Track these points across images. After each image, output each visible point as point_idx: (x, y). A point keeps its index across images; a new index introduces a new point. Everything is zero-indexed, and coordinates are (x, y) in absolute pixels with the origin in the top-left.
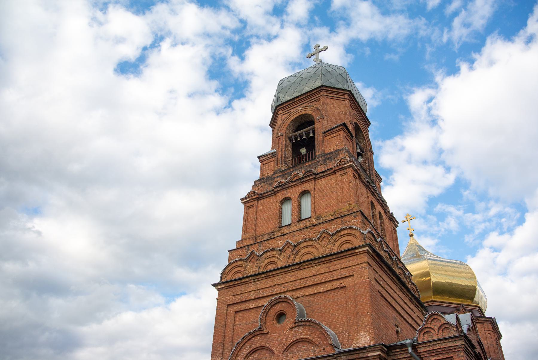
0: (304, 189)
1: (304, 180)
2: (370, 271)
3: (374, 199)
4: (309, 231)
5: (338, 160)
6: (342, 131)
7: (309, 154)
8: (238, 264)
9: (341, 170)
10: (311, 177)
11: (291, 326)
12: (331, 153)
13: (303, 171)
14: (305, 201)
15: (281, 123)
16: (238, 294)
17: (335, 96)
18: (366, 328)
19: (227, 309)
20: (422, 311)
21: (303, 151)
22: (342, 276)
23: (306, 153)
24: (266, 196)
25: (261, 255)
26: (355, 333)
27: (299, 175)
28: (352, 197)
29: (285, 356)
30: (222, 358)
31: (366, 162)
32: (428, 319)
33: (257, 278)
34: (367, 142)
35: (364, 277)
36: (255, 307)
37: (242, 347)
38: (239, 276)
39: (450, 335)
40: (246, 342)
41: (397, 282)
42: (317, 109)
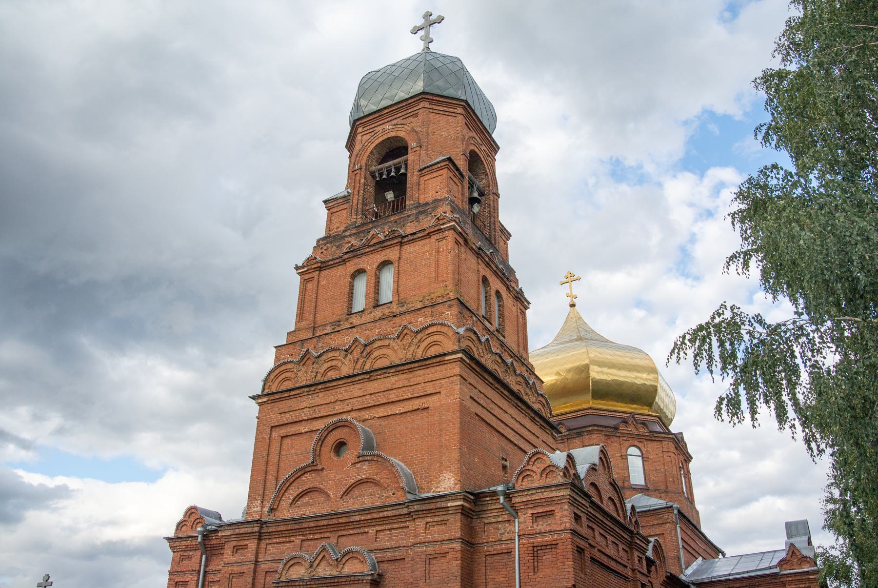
0: (383, 259)
1: (386, 244)
2: (464, 387)
3: (489, 271)
5: (436, 216)
6: (446, 170)
7: (398, 201)
10: (396, 241)
11: (353, 461)
12: (427, 204)
13: (386, 229)
15: (360, 148)
17: (442, 109)
18: (450, 467)
19: (271, 433)
20: (552, 434)
21: (390, 196)
22: (426, 393)
23: (393, 199)
24: (332, 265)
25: (319, 357)
26: (437, 473)
27: (379, 235)
28: (450, 276)
30: (262, 502)
31: (487, 210)
32: (531, 458)
33: (312, 389)
34: (490, 179)
35: (454, 395)
37: (288, 487)
38: (288, 385)
39: (555, 482)
40: (293, 481)
41: (510, 397)
42: (413, 130)
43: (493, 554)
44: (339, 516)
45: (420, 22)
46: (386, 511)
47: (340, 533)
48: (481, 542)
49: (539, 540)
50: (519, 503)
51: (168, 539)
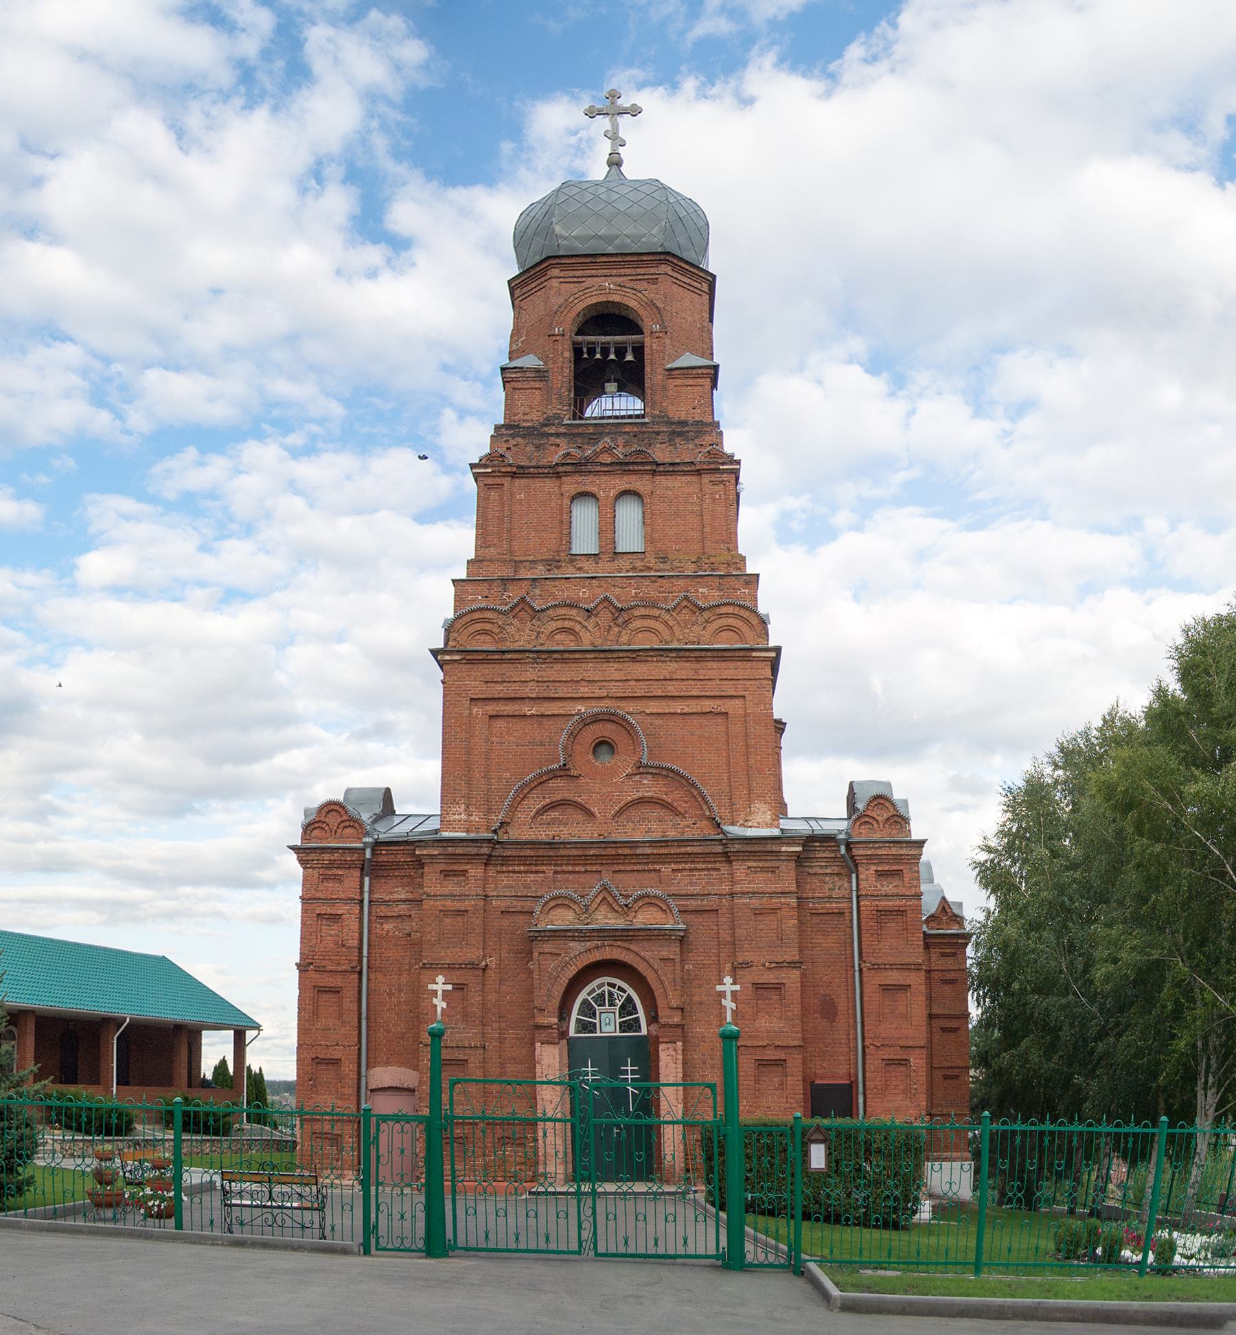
0: (628, 487)
8: (485, 616)
11: (629, 770)
16: (497, 682)
17: (688, 281)
22: (723, 694)
33: (543, 657)
44: (618, 845)
47: (616, 868)
48: (804, 895)
49: (885, 904)
51: (293, 848)
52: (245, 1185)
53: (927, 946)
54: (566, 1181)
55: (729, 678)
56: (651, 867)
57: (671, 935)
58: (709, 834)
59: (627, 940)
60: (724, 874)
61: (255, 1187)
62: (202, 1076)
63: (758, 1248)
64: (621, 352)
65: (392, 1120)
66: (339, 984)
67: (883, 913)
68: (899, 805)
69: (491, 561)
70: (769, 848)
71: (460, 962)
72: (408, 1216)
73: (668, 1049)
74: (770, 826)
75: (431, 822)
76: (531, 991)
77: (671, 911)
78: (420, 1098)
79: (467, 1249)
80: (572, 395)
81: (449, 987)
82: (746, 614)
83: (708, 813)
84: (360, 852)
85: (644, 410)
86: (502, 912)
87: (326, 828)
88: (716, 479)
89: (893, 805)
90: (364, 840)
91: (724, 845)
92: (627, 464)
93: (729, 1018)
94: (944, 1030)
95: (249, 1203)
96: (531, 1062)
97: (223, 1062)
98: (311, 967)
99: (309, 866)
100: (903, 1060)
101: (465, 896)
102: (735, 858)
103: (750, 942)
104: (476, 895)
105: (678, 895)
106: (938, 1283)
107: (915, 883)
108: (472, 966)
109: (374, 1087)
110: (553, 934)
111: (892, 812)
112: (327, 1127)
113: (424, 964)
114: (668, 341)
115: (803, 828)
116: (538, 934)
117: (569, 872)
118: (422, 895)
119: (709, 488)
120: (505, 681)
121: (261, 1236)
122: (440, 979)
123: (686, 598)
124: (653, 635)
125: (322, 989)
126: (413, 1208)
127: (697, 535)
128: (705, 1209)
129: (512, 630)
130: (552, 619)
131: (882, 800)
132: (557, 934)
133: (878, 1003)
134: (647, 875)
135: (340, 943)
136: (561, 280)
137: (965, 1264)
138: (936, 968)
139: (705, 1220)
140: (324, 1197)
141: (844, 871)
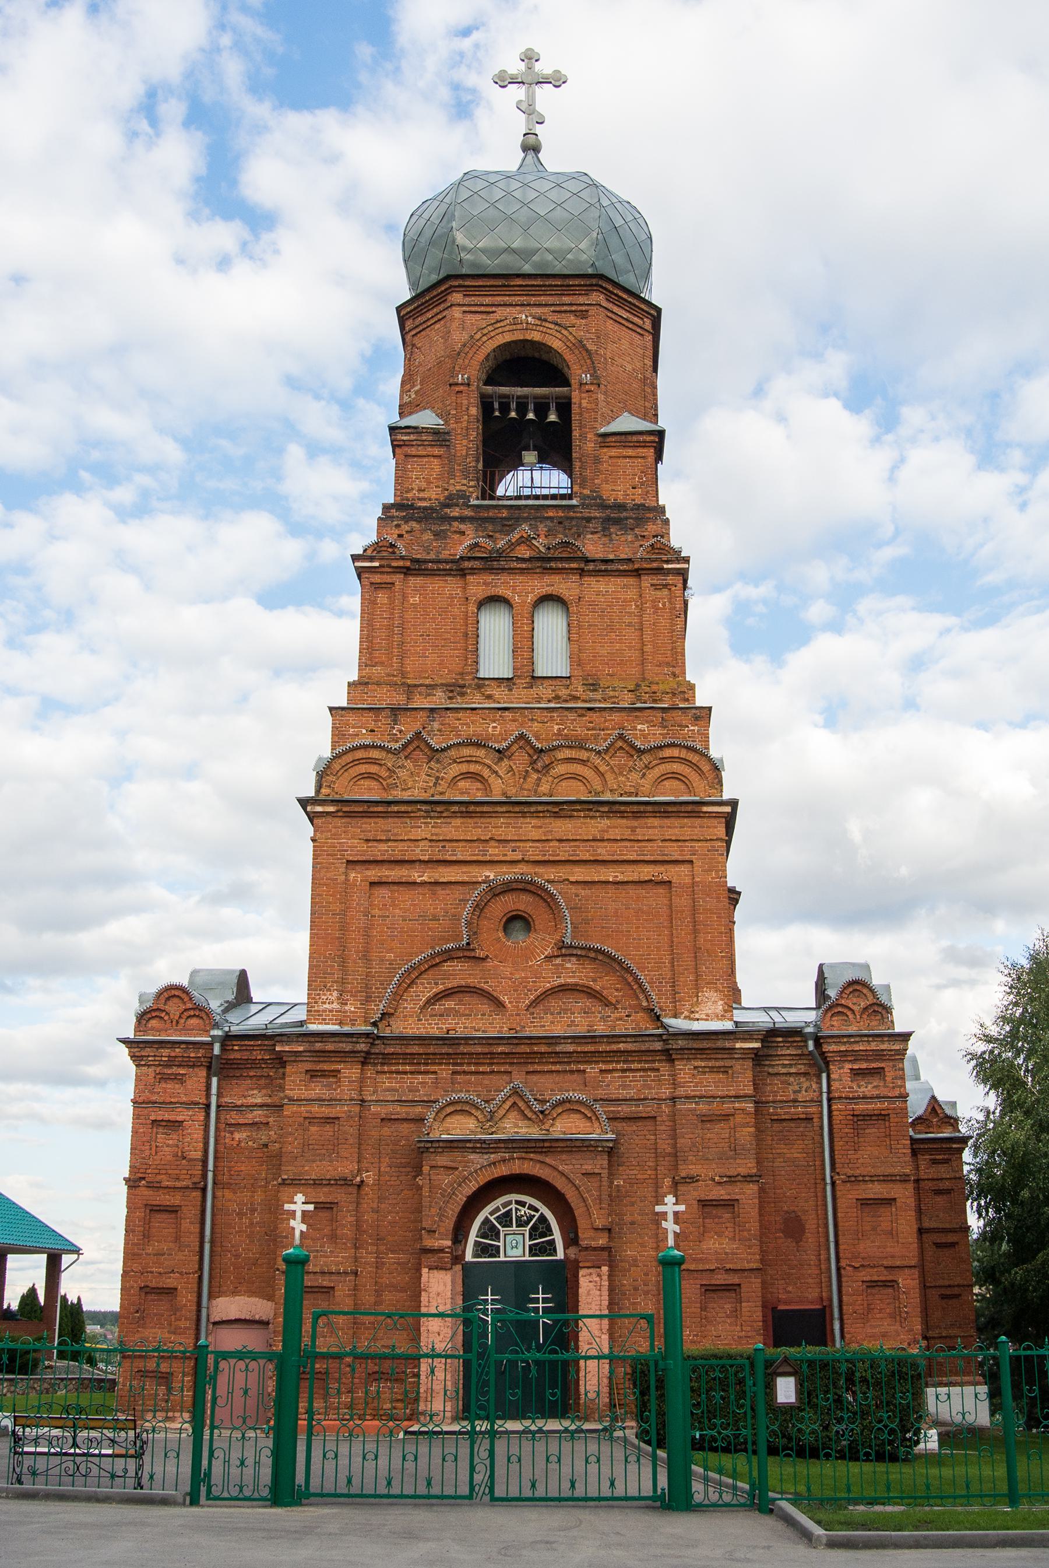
0: (549, 590)
4: (575, 720)
9: (655, 572)
10: (574, 565)
14: (541, 614)
16: (381, 840)
17: (626, 315)
18: (716, 984)
22: (666, 858)
29: (533, 1018)
33: (438, 809)
36: (430, 881)
42: (581, 344)
43: (785, 1120)
44: (533, 1041)
45: (516, 67)
46: (623, 1042)
47: (531, 1068)
49: (861, 1107)
50: (834, 1052)
51: (125, 1041)
52: (42, 1431)
53: (914, 1153)
54: (455, 1419)
55: (674, 838)
56: (573, 1067)
57: (597, 1147)
58: (646, 1029)
59: (542, 1152)
60: (665, 1075)
61: (56, 1432)
62: (5, 1307)
63: (710, 1488)
64: (542, 409)
65: (234, 1357)
66: (177, 1202)
67: (861, 1119)
68: (880, 992)
69: (378, 684)
70: (720, 1044)
71: (328, 1177)
72: (250, 1462)
73: (591, 1274)
74: (723, 1018)
75: (294, 1012)
76: (419, 1210)
77: (597, 1119)
78: (274, 1332)
79: (322, 1495)
80: (480, 466)
81: (311, 1207)
82: (695, 758)
83: (645, 1004)
84: (207, 1047)
85: (572, 488)
86: (382, 1120)
87: (166, 1018)
88: (658, 582)
89: (871, 990)
90: (212, 1033)
91: (664, 1041)
92: (550, 560)
93: (671, 1242)
94: (938, 1245)
95: (46, 1450)
96: (415, 1290)
97: (33, 1291)
98: (143, 1182)
99: (143, 1063)
100: (889, 1281)
101: (336, 1100)
102: (679, 1057)
103: (695, 1154)
104: (351, 1100)
105: (606, 1100)
106: (961, 1517)
107: (899, 1082)
108: (344, 1182)
109: (217, 1319)
110: (448, 1145)
111: (871, 1000)
112: (151, 1365)
113: (283, 1180)
114: (601, 397)
115: (762, 1020)
116: (429, 1145)
117: (472, 1073)
118: (283, 1099)
119: (650, 594)
120: (390, 840)
121: (71, 1488)
122: (300, 1198)
123: (621, 737)
124: (579, 783)
125: (155, 1208)
126: (258, 1453)
127: (635, 655)
128: (639, 1448)
129: (402, 774)
130: (455, 762)
131: (858, 986)
132: (453, 1145)
133: (856, 1219)
134: (568, 1077)
135: (180, 1154)
136: (464, 308)
137: (994, 1496)
138: (924, 1177)
139: (638, 1460)
140: (144, 1443)
141: (812, 1071)
